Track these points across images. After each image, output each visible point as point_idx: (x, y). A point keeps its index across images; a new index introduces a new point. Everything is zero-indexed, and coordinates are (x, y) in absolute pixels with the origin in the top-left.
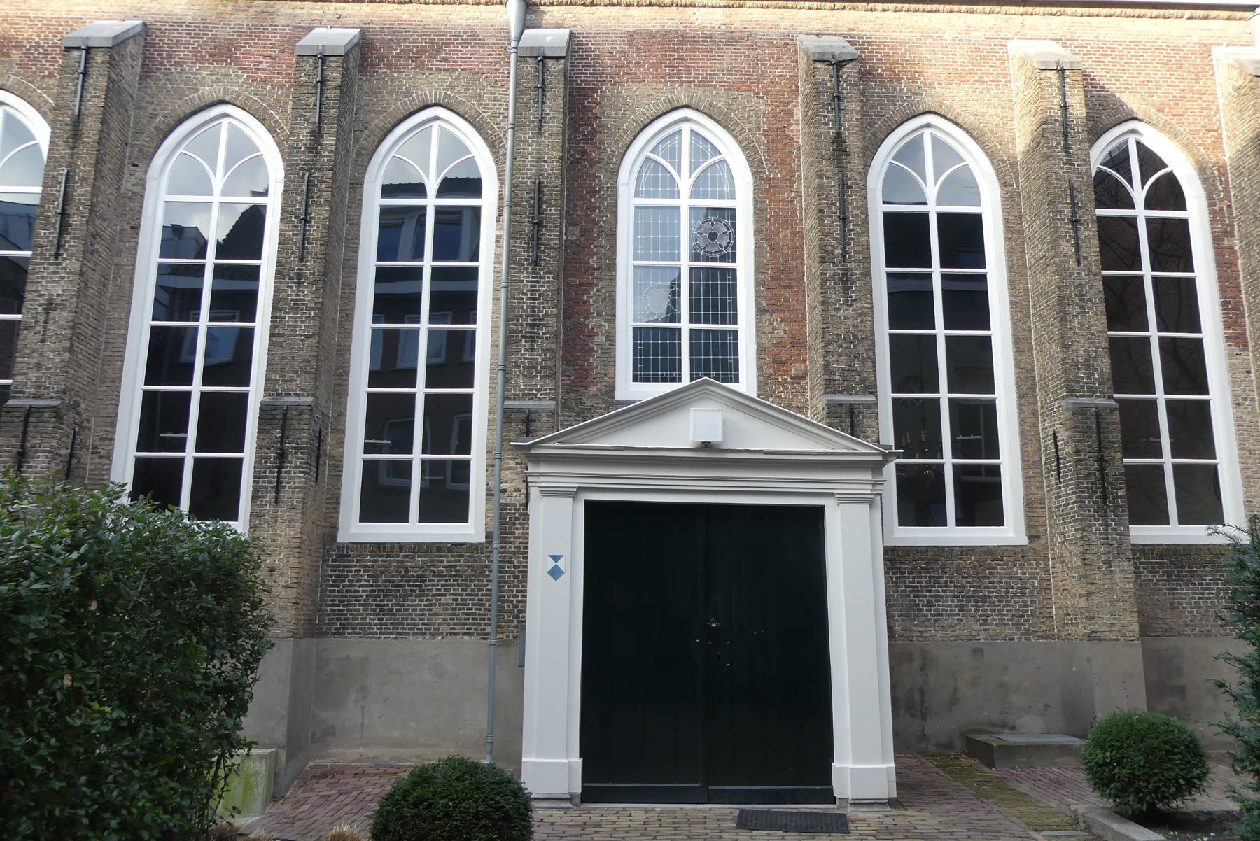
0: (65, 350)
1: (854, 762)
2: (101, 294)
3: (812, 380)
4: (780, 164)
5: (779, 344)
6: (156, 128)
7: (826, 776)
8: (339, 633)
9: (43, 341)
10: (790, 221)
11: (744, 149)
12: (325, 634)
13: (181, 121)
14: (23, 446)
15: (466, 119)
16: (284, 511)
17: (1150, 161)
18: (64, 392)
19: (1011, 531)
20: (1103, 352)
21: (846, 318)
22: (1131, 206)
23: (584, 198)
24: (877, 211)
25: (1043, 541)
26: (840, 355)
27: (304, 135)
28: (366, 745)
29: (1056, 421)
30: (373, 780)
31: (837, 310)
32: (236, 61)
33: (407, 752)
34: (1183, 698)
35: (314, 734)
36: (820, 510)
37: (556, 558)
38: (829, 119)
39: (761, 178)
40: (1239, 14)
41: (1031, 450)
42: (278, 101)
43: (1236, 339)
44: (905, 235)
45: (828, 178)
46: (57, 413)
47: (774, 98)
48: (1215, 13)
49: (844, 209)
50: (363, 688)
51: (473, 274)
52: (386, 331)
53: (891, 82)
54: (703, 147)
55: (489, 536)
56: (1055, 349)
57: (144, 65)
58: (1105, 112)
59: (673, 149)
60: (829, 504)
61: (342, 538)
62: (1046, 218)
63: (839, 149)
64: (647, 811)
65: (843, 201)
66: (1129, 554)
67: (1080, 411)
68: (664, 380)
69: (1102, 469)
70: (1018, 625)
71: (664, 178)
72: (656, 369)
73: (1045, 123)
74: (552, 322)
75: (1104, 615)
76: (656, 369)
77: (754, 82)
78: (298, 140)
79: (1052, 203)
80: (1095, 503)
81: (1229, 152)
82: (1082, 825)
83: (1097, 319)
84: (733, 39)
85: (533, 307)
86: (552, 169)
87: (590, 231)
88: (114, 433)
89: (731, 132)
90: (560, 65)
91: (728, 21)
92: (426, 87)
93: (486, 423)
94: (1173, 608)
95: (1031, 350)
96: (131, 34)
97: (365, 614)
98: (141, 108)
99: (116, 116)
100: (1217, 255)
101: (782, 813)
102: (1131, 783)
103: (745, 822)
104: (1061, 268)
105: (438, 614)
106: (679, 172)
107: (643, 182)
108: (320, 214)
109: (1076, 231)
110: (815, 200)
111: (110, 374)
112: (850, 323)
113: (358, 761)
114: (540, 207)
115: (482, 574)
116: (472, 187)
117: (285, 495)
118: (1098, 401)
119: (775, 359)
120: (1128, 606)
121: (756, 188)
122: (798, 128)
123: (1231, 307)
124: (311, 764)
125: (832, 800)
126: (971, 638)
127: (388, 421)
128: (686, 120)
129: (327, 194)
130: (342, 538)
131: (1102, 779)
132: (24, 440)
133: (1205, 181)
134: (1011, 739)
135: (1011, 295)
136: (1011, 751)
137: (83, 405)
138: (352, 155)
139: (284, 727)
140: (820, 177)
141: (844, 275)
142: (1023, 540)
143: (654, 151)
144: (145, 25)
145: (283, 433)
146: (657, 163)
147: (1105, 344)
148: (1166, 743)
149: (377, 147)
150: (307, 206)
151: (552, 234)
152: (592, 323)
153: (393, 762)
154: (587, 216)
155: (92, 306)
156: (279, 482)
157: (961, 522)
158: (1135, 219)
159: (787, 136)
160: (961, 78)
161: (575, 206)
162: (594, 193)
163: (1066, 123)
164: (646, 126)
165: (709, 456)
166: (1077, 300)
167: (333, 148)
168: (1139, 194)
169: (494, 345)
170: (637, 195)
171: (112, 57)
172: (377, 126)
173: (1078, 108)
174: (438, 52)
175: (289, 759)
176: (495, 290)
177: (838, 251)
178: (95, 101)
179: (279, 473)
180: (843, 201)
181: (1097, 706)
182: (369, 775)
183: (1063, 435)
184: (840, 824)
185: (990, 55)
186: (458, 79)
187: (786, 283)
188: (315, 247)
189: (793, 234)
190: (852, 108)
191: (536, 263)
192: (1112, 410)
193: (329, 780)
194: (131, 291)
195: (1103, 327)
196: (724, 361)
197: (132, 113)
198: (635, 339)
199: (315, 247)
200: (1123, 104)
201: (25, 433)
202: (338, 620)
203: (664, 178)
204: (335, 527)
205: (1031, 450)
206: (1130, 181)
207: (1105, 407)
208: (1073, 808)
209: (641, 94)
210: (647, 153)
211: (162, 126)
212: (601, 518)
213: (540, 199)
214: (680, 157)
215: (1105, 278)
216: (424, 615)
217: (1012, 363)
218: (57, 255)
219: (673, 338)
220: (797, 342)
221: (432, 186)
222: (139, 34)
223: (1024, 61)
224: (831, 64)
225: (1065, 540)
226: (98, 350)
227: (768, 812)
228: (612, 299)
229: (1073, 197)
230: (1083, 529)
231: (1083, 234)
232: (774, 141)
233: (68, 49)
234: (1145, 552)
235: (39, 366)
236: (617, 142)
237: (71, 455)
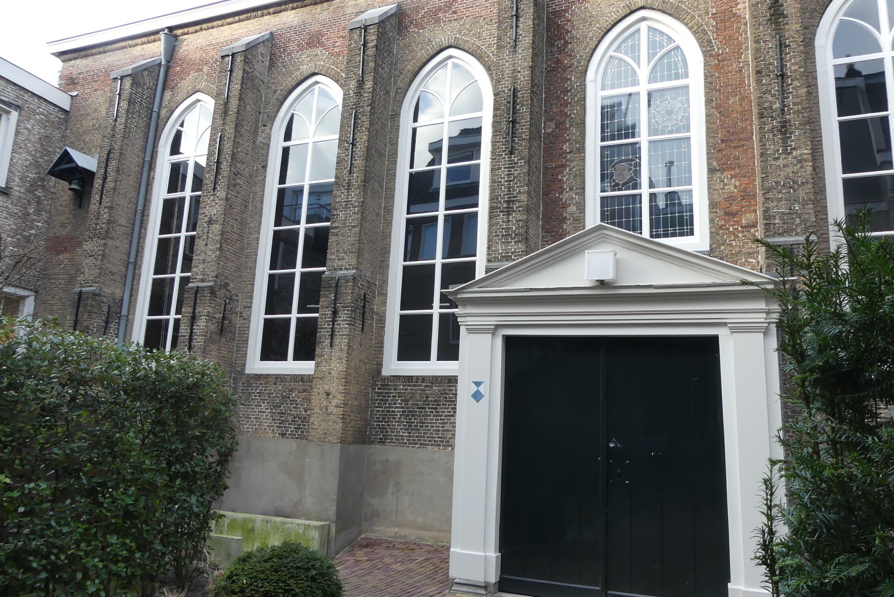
0: (217, 250)
1: (747, 585)
2: (242, 212)
4: (728, 40)
5: (731, 198)
6: (277, 99)
8: (382, 442)
9: (206, 245)
11: (695, 33)
12: (373, 442)
13: (290, 92)
14: (194, 312)
15: (470, 53)
16: (336, 352)
18: (217, 277)
22: (879, 50)
23: (558, 97)
24: (828, 66)
26: (780, 200)
28: (399, 526)
32: (322, 44)
33: (427, 534)
35: (365, 515)
36: (714, 340)
37: (478, 384)
39: (711, 55)
45: (765, 41)
46: (212, 291)
49: (782, 66)
50: (397, 483)
57: (270, 59)
60: (724, 335)
61: (385, 372)
74: (524, 197)
85: (509, 188)
86: (524, 77)
87: (564, 123)
88: (251, 303)
89: (682, 21)
92: (441, 36)
96: (261, 40)
97: (398, 428)
98: (269, 88)
99: (250, 95)
105: (449, 431)
106: (639, 64)
107: (609, 77)
111: (250, 264)
112: (790, 170)
113: (394, 537)
114: (514, 108)
117: (337, 341)
119: (724, 211)
121: (706, 64)
124: (363, 536)
127: (416, 287)
128: (644, 19)
130: (385, 372)
132: (194, 309)
137: (231, 285)
138: (392, 94)
139: (334, 508)
141: (782, 127)
144: (271, 33)
145: (335, 296)
146: (621, 59)
151: (524, 129)
152: (565, 196)
153: (417, 541)
155: (236, 220)
156: (333, 331)
159: (735, 15)
161: (551, 105)
162: (566, 92)
165: (605, 292)
171: (246, 57)
172: (409, 71)
174: (450, 8)
175: (338, 531)
177: (777, 105)
178: (236, 87)
179: (333, 325)
186: (464, 24)
187: (736, 143)
189: (742, 99)
191: (511, 153)
193: (368, 550)
194: (262, 209)
197: (263, 92)
198: (602, 206)
199: (359, 162)
201: (195, 304)
202: (382, 432)
204: (380, 365)
211: (280, 97)
213: (514, 102)
216: (439, 431)
218: (214, 189)
222: (267, 40)
226: (242, 249)
228: (582, 176)
232: (722, 21)
233: (223, 57)
235: (204, 260)
236: (585, 48)
237: (224, 318)
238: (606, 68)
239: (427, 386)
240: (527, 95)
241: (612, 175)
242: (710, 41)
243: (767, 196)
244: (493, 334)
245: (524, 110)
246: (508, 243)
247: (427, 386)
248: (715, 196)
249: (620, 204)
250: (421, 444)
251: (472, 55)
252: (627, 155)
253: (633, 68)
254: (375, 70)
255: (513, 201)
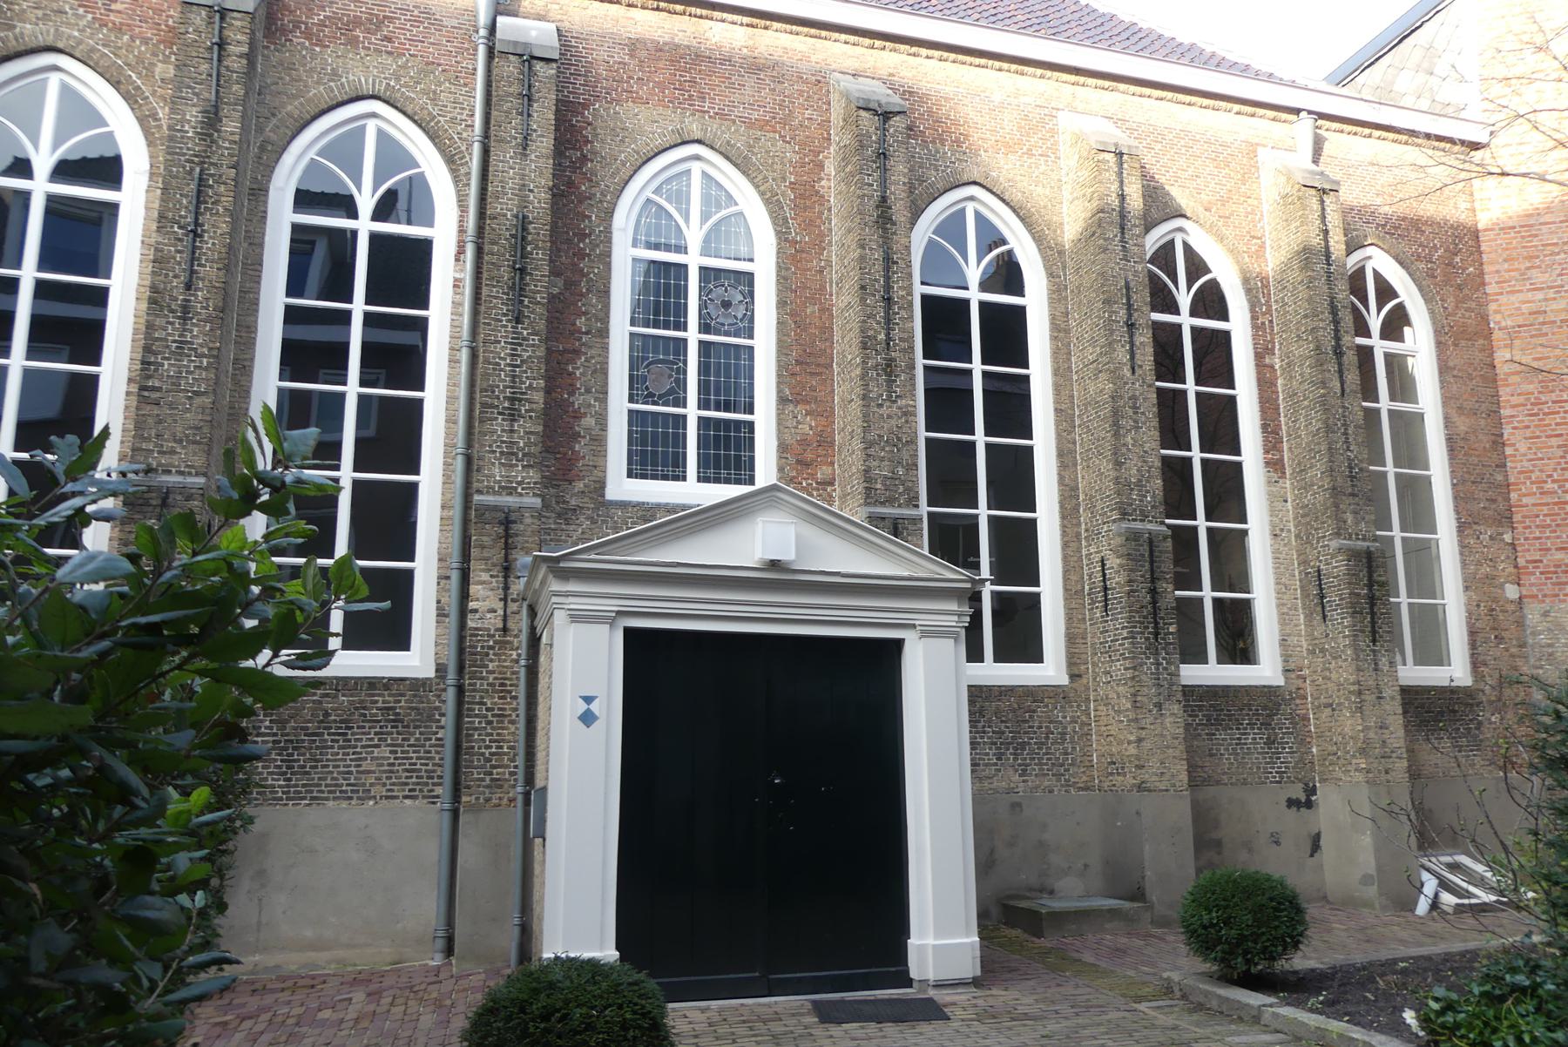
1: (936, 938)
3: (843, 487)
4: (809, 225)
5: (804, 442)
7: (898, 953)
10: (819, 294)
11: (767, 202)
15: (415, 122)
17: (1197, 267)
19: (1050, 670)
20: (1156, 472)
21: (889, 417)
22: (1177, 312)
23: (569, 241)
25: (1084, 681)
27: (193, 115)
29: (1106, 548)
30: (285, 996)
31: (880, 406)
33: (321, 957)
34: (1219, 853)
36: (899, 644)
37: (588, 700)
38: (873, 179)
39: (786, 240)
40: (1284, 116)
41: (1074, 578)
42: (140, 60)
43: (1274, 465)
44: (944, 321)
47: (802, 144)
48: (1122, 86)
49: (888, 287)
50: (261, 873)
51: (100, 297)
52: (293, 391)
53: (933, 142)
54: (716, 195)
55: (441, 669)
56: (1106, 466)
58: (1160, 207)
59: (679, 192)
62: (1100, 318)
63: (884, 219)
64: (703, 1010)
65: (887, 278)
66: (1179, 696)
67: (1133, 536)
68: (728, 481)
69: (1154, 602)
70: (1058, 776)
71: (668, 227)
72: (655, 464)
73: (1102, 211)
75: (1154, 764)
76: (655, 464)
77: (777, 123)
78: (183, 121)
79: (1107, 302)
80: (1147, 639)
81: (1272, 262)
82: (1178, 994)
83: (1149, 434)
84: (756, 67)
85: (514, 377)
86: (539, 201)
89: (752, 180)
90: (551, 70)
91: (751, 43)
92: (360, 70)
93: (438, 522)
94: (1211, 755)
95: (1075, 465)
100: (1258, 373)
101: (866, 1002)
102: (1238, 945)
103: (828, 1015)
104: (1115, 375)
105: (369, 772)
106: (687, 220)
108: (217, 229)
109: (1131, 336)
110: (855, 275)
112: (893, 422)
113: (252, 973)
115: (431, 718)
116: (107, 170)
118: (1150, 526)
119: (802, 459)
120: (1177, 753)
122: (831, 182)
123: (1270, 429)
125: (908, 982)
126: (1010, 791)
128: (697, 158)
129: (227, 200)
131: (1203, 940)
133: (1248, 291)
134: (1057, 905)
135: (1056, 402)
136: (1060, 918)
140: (863, 247)
141: (888, 366)
142: (1064, 680)
143: (657, 191)
146: (660, 207)
147: (1158, 464)
148: (1271, 899)
149: (289, 143)
150: (197, 214)
153: (303, 972)
154: (574, 264)
157: (999, 657)
158: (1180, 326)
160: (1009, 148)
161: (559, 250)
162: (583, 236)
163: (1123, 214)
164: (649, 160)
165: (777, 577)
166: (1130, 412)
167: (237, 138)
168: (1184, 299)
169: (451, 420)
170: (634, 245)
172: (290, 115)
173: (1135, 202)
174: (379, 28)
176: (452, 349)
177: (882, 336)
180: (887, 278)
181: (1146, 864)
182: (273, 991)
183: (1113, 562)
184: (929, 1011)
185: (1040, 124)
186: (404, 66)
187: (813, 368)
188: (209, 271)
189: (822, 310)
190: (899, 170)
191: (518, 320)
192: (1165, 538)
195: (1156, 445)
196: (738, 458)
198: (630, 424)
199: (209, 271)
200: (1172, 199)
203: (668, 227)
205: (1074, 578)
206: (1176, 283)
207: (1158, 533)
208: (1165, 975)
209: (644, 118)
210: (648, 193)
212: (644, 651)
213: (523, 238)
214: (688, 203)
215: (1160, 391)
217: (1055, 478)
219: (676, 426)
220: (824, 441)
221: (43, 163)
223: (1078, 138)
224: (875, 113)
225: (1114, 679)
227: (842, 1001)
229: (1129, 299)
230: (1134, 668)
231: (1138, 340)
232: (802, 196)
234: (1189, 691)
236: (613, 175)
238: (640, 216)
239: (327, 695)
240: (544, 232)
241: (645, 379)
242: (785, 220)
243: (869, 452)
244: (611, 625)
245: (539, 255)
246: (512, 466)
247: (327, 695)
248: (787, 436)
249: (655, 425)
250: (313, 798)
251: (420, 126)
252: (666, 353)
253: (678, 225)
254: (245, 101)
255: (520, 400)
